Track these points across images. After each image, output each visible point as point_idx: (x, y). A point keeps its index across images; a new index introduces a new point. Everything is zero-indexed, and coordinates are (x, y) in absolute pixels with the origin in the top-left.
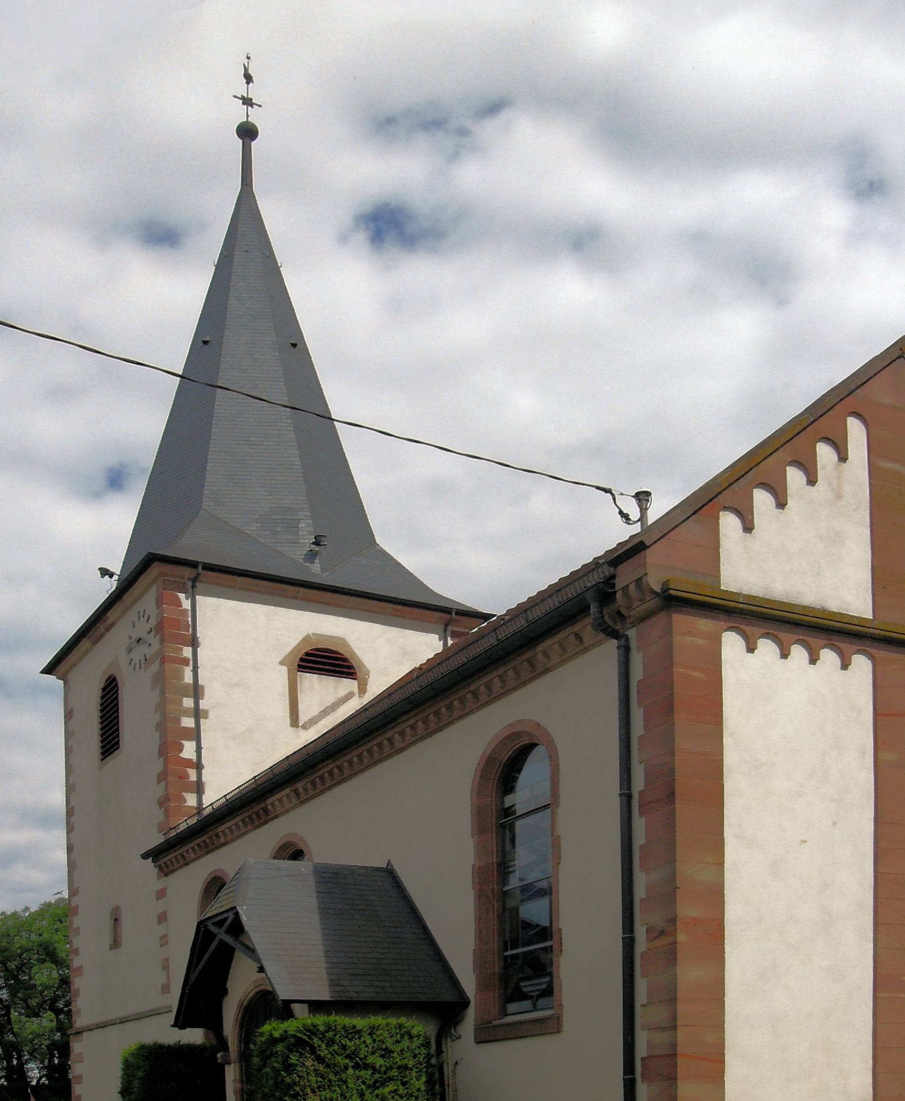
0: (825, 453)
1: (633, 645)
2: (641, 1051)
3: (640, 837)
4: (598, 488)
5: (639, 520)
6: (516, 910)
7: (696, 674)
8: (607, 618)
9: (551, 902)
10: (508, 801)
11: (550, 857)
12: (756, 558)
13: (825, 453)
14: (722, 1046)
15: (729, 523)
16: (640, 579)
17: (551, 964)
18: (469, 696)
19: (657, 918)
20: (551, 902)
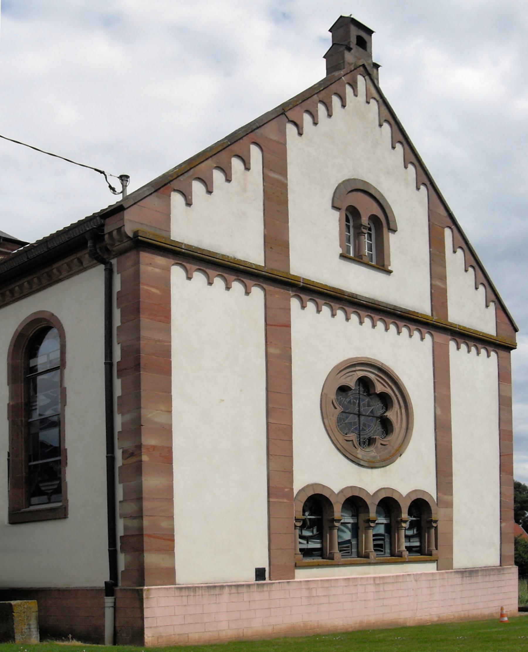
0: (236, 164)
1: (115, 269)
2: (120, 532)
3: (118, 392)
4: (96, 170)
5: (121, 193)
6: (37, 434)
7: (154, 290)
8: (98, 250)
9: (60, 431)
10: (32, 363)
11: (60, 401)
12: (190, 223)
13: (236, 164)
14: (173, 530)
15: (177, 199)
16: (120, 228)
17: (60, 473)
18: (8, 293)
19: (128, 444)
20: (60, 431)
